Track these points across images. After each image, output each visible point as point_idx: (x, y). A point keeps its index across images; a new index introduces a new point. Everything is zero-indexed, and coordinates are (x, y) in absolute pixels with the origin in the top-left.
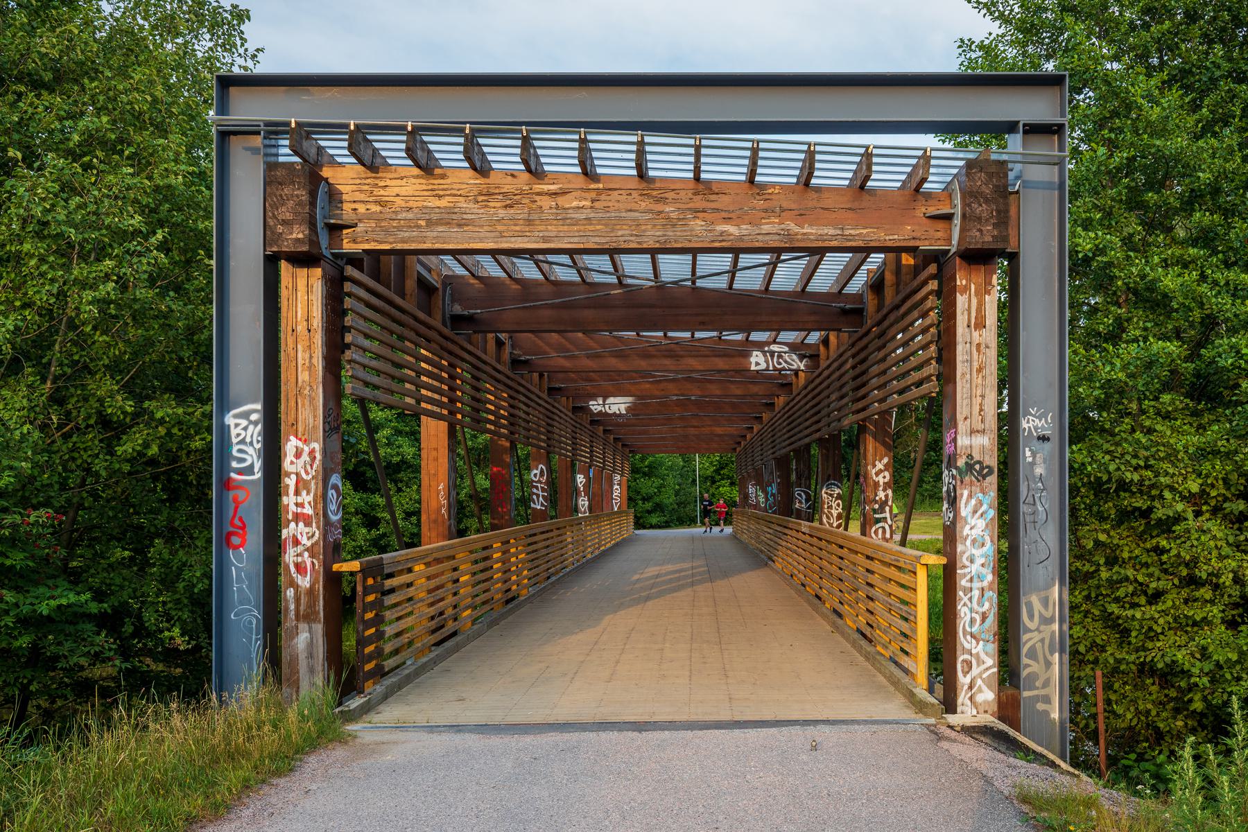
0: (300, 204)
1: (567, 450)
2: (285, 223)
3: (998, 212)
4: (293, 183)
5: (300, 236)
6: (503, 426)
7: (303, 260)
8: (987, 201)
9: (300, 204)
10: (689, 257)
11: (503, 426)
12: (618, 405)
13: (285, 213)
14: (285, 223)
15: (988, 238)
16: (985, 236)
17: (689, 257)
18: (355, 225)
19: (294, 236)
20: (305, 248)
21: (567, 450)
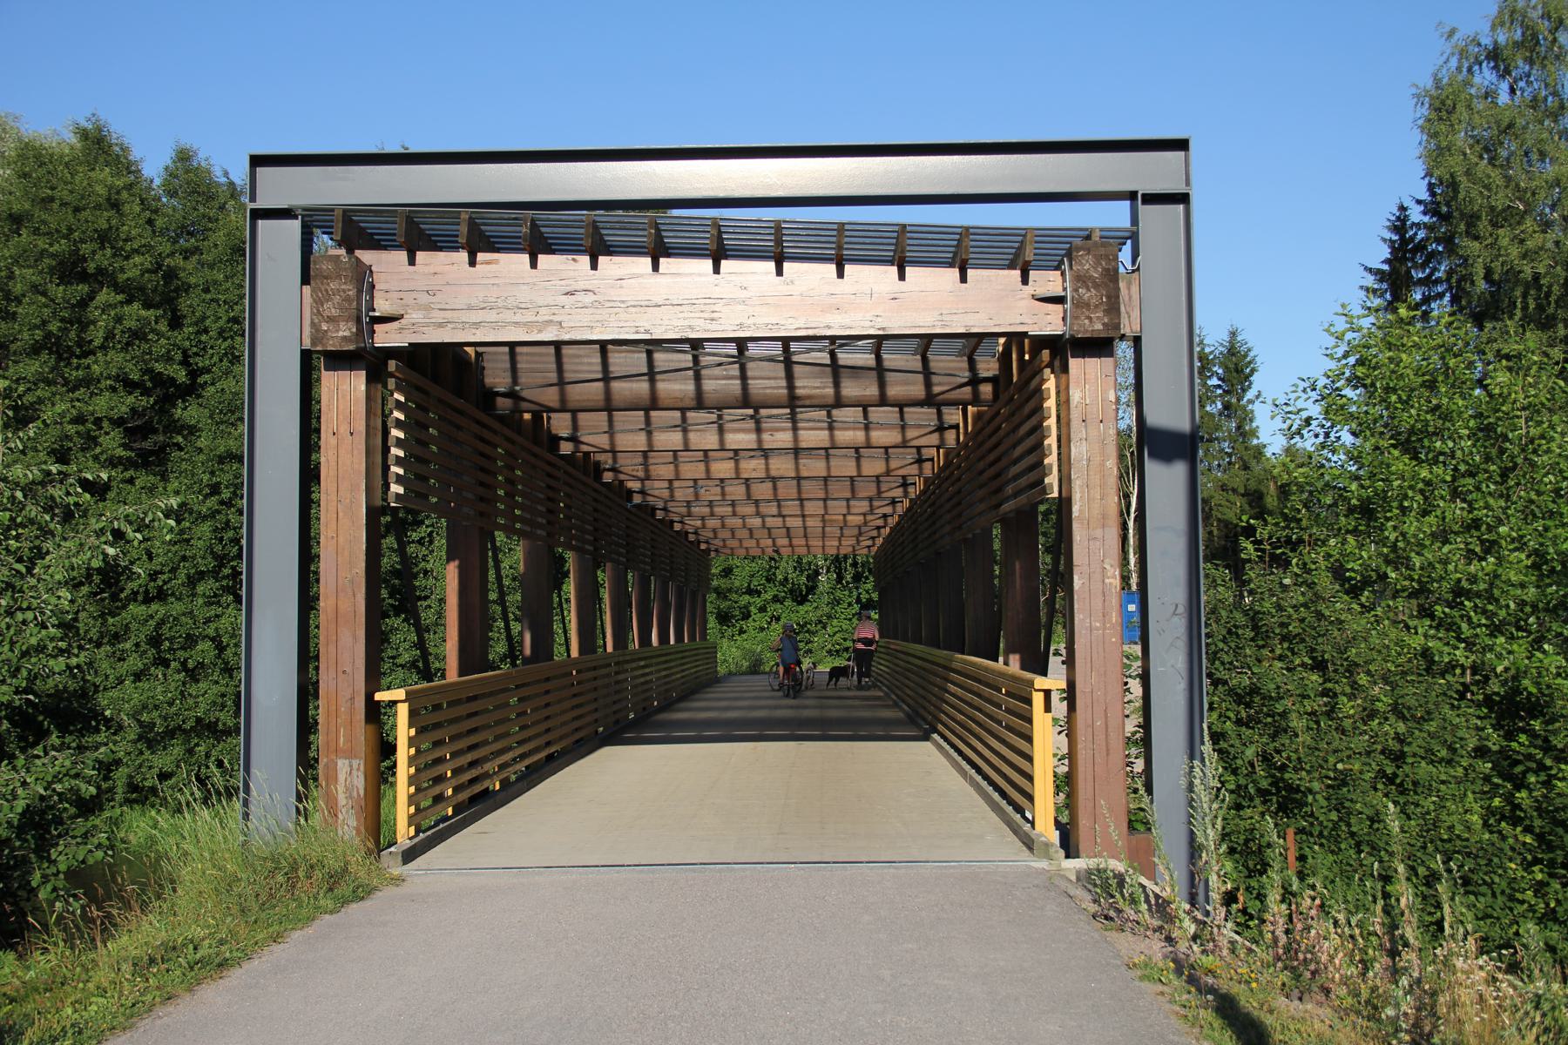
0: (348, 299)
1: (620, 554)
2: (331, 319)
3: (1108, 297)
4: (339, 277)
5: (347, 334)
6: (540, 526)
7: (340, 360)
8: (1096, 286)
9: (348, 299)
10: (645, 370)
11: (540, 526)
12: (434, 500)
13: (330, 309)
14: (331, 319)
15: (1099, 326)
16: (1095, 325)
17: (645, 370)
18: (402, 316)
19: (341, 334)
20: (352, 347)
21: (620, 554)
